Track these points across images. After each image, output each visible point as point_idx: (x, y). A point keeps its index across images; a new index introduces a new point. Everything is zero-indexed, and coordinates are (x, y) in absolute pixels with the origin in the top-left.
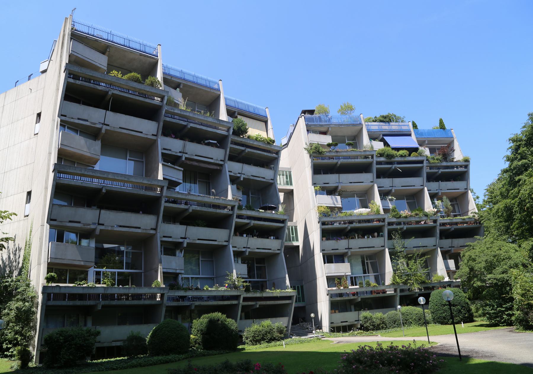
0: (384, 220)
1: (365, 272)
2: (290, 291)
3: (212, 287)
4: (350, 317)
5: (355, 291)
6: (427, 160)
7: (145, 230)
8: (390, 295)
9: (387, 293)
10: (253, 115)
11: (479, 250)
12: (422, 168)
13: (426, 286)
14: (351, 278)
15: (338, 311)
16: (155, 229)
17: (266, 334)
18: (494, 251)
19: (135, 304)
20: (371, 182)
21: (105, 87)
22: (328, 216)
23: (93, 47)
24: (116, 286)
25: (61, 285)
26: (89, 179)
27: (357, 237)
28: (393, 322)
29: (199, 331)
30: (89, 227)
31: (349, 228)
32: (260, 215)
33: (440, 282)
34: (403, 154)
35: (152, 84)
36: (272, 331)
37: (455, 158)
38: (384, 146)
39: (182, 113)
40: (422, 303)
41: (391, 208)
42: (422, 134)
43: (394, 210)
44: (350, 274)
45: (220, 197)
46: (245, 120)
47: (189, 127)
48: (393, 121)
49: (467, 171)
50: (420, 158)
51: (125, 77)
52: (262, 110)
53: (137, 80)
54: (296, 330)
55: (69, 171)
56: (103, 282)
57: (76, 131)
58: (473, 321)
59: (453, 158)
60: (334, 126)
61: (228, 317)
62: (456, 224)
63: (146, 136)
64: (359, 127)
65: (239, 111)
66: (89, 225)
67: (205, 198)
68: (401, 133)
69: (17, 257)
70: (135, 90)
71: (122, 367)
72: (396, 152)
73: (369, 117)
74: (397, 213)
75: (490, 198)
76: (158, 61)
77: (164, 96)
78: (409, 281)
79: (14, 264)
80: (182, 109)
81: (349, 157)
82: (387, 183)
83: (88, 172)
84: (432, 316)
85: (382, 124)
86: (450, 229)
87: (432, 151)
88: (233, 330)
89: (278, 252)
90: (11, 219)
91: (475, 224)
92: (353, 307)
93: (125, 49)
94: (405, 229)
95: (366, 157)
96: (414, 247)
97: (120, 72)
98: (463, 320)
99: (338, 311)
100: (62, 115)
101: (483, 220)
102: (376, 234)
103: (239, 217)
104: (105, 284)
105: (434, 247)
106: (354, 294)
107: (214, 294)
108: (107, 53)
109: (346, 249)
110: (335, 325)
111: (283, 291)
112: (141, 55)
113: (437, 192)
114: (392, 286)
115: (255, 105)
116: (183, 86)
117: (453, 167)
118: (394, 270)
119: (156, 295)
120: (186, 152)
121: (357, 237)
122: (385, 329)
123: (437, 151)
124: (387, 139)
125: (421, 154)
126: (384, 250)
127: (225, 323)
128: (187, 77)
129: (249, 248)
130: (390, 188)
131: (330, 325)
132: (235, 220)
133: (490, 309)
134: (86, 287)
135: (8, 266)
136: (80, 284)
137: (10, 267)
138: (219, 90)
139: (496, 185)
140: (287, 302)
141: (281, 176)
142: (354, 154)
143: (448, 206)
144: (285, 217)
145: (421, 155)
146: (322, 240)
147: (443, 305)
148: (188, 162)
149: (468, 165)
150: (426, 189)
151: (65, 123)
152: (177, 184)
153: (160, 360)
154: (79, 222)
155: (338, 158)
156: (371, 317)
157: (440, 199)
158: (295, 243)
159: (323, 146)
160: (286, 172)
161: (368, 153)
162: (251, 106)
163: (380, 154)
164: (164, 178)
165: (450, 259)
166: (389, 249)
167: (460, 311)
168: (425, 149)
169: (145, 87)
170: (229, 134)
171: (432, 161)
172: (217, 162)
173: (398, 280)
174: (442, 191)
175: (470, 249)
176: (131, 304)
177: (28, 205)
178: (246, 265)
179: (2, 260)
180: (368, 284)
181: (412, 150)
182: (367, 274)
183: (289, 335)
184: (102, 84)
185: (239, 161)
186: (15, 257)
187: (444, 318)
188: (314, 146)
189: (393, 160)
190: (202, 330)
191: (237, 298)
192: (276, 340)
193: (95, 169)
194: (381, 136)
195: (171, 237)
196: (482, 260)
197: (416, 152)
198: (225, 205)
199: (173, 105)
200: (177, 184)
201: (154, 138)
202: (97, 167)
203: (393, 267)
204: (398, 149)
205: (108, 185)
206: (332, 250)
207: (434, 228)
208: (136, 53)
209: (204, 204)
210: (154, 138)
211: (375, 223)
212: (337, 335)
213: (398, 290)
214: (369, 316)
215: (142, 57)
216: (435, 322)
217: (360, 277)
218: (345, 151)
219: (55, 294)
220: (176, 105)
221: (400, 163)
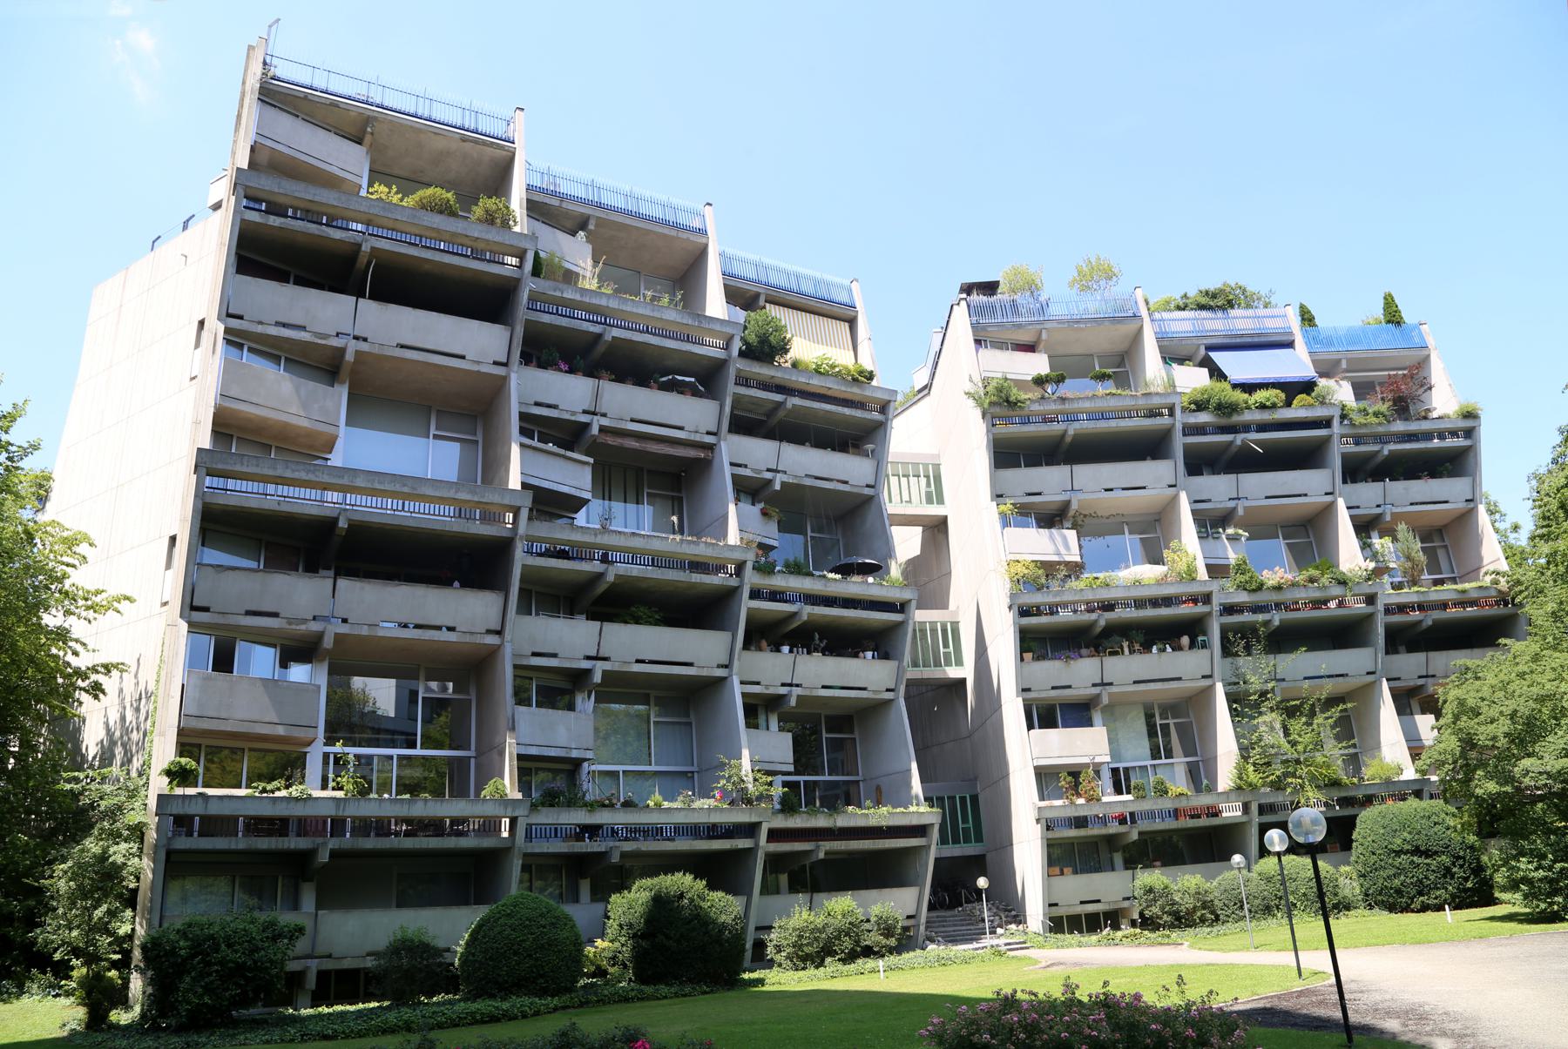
0: (1207, 598)
1: (1155, 754)
2: (920, 811)
3: (673, 800)
4: (1110, 887)
5: (1126, 811)
6: (1343, 417)
7: (468, 635)
8: (1229, 822)
9: (1224, 815)
10: (812, 303)
11: (1494, 682)
12: (1326, 441)
13: (1344, 794)
14: (1115, 771)
15: (1070, 869)
16: (499, 633)
17: (838, 938)
18: (1539, 684)
19: (430, 846)
20: (1170, 486)
21: (364, 233)
22: (1039, 589)
23: (328, 124)
24: (373, 796)
25: (211, 792)
26: (313, 494)
27: (1126, 650)
28: (1235, 904)
29: (622, 928)
30: (303, 627)
31: (1102, 623)
32: (829, 589)
33: (1388, 782)
34: (1268, 400)
35: (493, 219)
36: (858, 928)
37: (1435, 409)
38: (1211, 377)
39: (587, 300)
40: (1277, 848)
41: (1233, 562)
42: (1329, 341)
43: (1241, 568)
44: (1108, 759)
45: (699, 538)
46: (773, 311)
47: (608, 337)
48: (1239, 305)
49: (1471, 446)
50: (1319, 412)
51: (410, 201)
52: (841, 287)
53: (445, 210)
54: (950, 926)
55: (238, 468)
56: (334, 784)
57: (276, 359)
58: (1490, 901)
59: (1429, 410)
60: (1055, 325)
61: (712, 886)
62: (1444, 605)
63: (475, 368)
64: (1131, 327)
65: (769, 292)
66: (305, 621)
67: (655, 540)
68: (1263, 339)
69: (142, 718)
70: (439, 235)
71: (352, 1031)
72: (1246, 396)
73: (1165, 296)
74: (1251, 577)
75: (1543, 527)
76: (514, 154)
77: (525, 251)
78: (1290, 780)
79: (135, 736)
80: (587, 287)
81: (1103, 416)
82: (1219, 488)
83: (293, 471)
84: (1362, 885)
85: (1204, 314)
86: (1420, 622)
87: (1361, 390)
88: (724, 926)
89: (889, 696)
90: (118, 612)
91: (1499, 605)
92: (1118, 859)
93: (417, 125)
94: (1277, 623)
95: (1153, 413)
96: (1305, 678)
97: (394, 188)
98: (1459, 897)
99: (1070, 869)
100: (229, 315)
101: (1521, 592)
102: (1185, 640)
103: (755, 594)
104: (341, 789)
105: (1371, 678)
106: (1122, 820)
107: (680, 819)
108: (368, 139)
109: (1094, 685)
110: (1060, 912)
111: (898, 810)
112: (464, 139)
113: (1378, 511)
114: (1233, 796)
115: (818, 275)
116: (596, 226)
117: (1428, 436)
118: (1242, 748)
119: (500, 822)
120: (603, 411)
121: (1126, 650)
122: (1211, 925)
123: (1378, 389)
124: (1218, 357)
125: (1324, 398)
126: (1211, 688)
127: (702, 904)
128: (607, 199)
129: (797, 686)
130: (1232, 504)
131: (1047, 911)
132: (746, 605)
133: (1530, 867)
134: (284, 797)
135: (119, 743)
136: (264, 790)
137: (124, 745)
138: (702, 232)
139: (1548, 480)
140: (743, 843)
141: (913, 480)
142: (1113, 403)
143: (1413, 554)
144: (907, 595)
145: (1323, 403)
146: (1022, 659)
147: (1395, 851)
148: (611, 441)
149: (1474, 427)
150: (1341, 504)
151: (238, 336)
152: (576, 504)
153: (473, 1014)
154: (275, 615)
155: (1071, 417)
156: (1166, 887)
157: (1389, 532)
158: (953, 672)
159: (1020, 384)
160: (926, 466)
161: (1156, 401)
162: (808, 278)
163: (1196, 403)
164: (525, 486)
165: (1423, 712)
166: (1227, 684)
167: (1448, 872)
168: (1340, 386)
169: (471, 227)
170: (730, 356)
171: (1359, 419)
172: (697, 438)
173: (1253, 777)
174: (1395, 510)
175: (1466, 680)
176: (417, 846)
177: (168, 572)
178: (790, 735)
179: (107, 724)
180: (1162, 791)
181: (1294, 389)
182: (1164, 761)
183: (921, 939)
184: (354, 226)
185: (770, 435)
186: (137, 718)
187: (1399, 892)
188: (994, 384)
189: (1236, 419)
190: (630, 926)
191: (751, 830)
192: (875, 953)
193: (329, 463)
194: (1202, 351)
195: (554, 655)
196: (1501, 712)
197: (1309, 394)
198: (722, 562)
199: (560, 279)
200: (576, 504)
201: (500, 371)
202: (336, 459)
203: (1238, 737)
204: (1249, 388)
205: (413, 515)
206: (1053, 688)
207: (1369, 617)
208: (451, 134)
209: (658, 560)
210: (500, 371)
211: (1186, 610)
212: (1064, 940)
213: (1254, 808)
214: (1158, 886)
215: (468, 145)
216: (1370, 905)
217: (1140, 767)
218: (1087, 398)
219: (205, 819)
220: (570, 277)
221: (1263, 427)
